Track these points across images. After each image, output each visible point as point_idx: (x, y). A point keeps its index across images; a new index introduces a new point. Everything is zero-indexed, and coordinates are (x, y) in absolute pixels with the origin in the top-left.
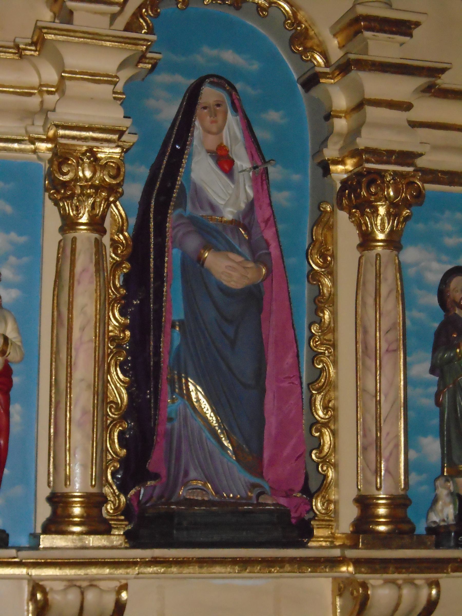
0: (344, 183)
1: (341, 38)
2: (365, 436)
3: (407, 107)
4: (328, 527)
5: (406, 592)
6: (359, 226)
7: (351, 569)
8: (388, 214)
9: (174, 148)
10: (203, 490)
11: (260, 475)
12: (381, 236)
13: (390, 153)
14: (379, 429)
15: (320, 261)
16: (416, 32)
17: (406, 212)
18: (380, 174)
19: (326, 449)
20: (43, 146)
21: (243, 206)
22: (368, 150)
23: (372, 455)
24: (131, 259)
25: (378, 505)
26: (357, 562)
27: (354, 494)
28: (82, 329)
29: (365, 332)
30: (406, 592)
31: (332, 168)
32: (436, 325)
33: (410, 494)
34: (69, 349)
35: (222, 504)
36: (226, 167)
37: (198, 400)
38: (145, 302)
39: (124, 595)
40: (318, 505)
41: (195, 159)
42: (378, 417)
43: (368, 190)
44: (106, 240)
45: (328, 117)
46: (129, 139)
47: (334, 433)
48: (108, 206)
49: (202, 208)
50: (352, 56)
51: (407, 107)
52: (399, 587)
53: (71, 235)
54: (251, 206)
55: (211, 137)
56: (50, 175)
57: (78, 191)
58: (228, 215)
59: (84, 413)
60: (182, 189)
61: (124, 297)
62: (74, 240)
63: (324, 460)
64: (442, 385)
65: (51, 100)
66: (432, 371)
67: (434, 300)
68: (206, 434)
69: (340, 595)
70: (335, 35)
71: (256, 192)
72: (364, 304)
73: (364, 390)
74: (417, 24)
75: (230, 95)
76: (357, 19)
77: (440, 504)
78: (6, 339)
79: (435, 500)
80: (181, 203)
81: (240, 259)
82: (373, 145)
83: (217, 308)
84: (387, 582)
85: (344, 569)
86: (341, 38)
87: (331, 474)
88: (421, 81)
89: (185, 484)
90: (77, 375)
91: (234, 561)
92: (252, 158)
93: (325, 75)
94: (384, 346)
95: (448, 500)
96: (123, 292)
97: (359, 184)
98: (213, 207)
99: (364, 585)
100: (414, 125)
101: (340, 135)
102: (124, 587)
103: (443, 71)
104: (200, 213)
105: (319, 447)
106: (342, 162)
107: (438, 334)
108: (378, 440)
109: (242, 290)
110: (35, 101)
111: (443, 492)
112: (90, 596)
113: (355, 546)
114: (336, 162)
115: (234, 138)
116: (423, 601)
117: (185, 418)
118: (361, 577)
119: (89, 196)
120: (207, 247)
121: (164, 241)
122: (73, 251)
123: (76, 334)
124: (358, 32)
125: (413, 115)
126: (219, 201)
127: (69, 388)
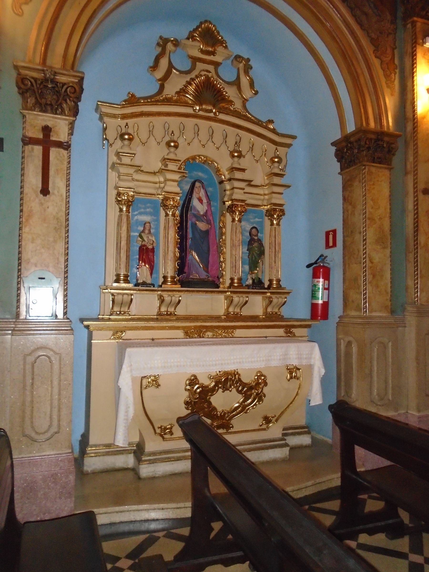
0: (229, 207)
1: (229, 172)
2: (232, 264)
3: (244, 189)
4: (223, 285)
5: (241, 299)
6: (232, 217)
7: (229, 293)
8: (239, 214)
9: (189, 197)
10: (196, 276)
11: (208, 273)
12: (237, 219)
13: (239, 200)
14: (236, 263)
15: (222, 224)
16: (285, 177)
17: (243, 214)
18: (238, 205)
19: (223, 268)
20: (160, 196)
21: (205, 211)
22: (234, 199)
23: (234, 269)
24: (180, 223)
25: (235, 280)
26: (231, 292)
27: (268, 279)
28: (171, 239)
29: (233, 241)
30: (241, 299)
31: (226, 203)
32: (249, 240)
33: (242, 278)
34: (168, 243)
35: (200, 279)
36: (201, 202)
37: (195, 256)
38: (183, 233)
39: (132, 297)
40: (221, 280)
41: (194, 199)
42: (236, 260)
43: (235, 209)
44: (130, 214)
45: (225, 191)
46: (181, 195)
47: (225, 264)
48: (176, 211)
49: (196, 211)
50: (232, 177)
51: (244, 189)
52: (240, 298)
53: (168, 217)
54: (207, 211)
55: (197, 194)
56: (162, 203)
57: (170, 207)
58: (202, 213)
59: (171, 258)
60: (191, 207)
61: (178, 232)
62: (169, 218)
63: (223, 270)
64: (249, 254)
65: (162, 185)
66: (247, 250)
67: (248, 234)
68: (197, 264)
69: (226, 300)
70: (227, 171)
71: (208, 207)
72: (233, 235)
73: (233, 254)
74: (246, 169)
75: (202, 185)
76: (233, 168)
77: (248, 280)
78: (153, 241)
79: (248, 279)
80: (191, 210)
81: (205, 224)
82: (236, 198)
83: (199, 235)
84: (237, 296)
85: (228, 293)
86: (229, 172)
87: (224, 273)
88: (247, 183)
89: (192, 275)
90: (170, 249)
91: (204, 291)
92: (207, 200)
93: (225, 181)
94: (237, 244)
95: (251, 279)
96: (178, 231)
97: (232, 207)
98: (198, 211)
99: (232, 297)
100: (245, 193)
101: (227, 195)
102: (181, 296)
103: (252, 181)
104: (195, 213)
105: (222, 267)
106: (228, 202)
107: (249, 242)
108: (236, 265)
109: (205, 231)
110: (157, 185)
111: (249, 277)
112: (173, 298)
113: (231, 288)
114: (227, 201)
115: (202, 195)
116: (245, 301)
117: (192, 260)
118: (232, 295)
119: (172, 208)
120: (198, 221)
121: (187, 219)
122: (169, 221)
123: (169, 240)
124: (233, 171)
125: (245, 191)
126: (200, 210)
127: (168, 253)
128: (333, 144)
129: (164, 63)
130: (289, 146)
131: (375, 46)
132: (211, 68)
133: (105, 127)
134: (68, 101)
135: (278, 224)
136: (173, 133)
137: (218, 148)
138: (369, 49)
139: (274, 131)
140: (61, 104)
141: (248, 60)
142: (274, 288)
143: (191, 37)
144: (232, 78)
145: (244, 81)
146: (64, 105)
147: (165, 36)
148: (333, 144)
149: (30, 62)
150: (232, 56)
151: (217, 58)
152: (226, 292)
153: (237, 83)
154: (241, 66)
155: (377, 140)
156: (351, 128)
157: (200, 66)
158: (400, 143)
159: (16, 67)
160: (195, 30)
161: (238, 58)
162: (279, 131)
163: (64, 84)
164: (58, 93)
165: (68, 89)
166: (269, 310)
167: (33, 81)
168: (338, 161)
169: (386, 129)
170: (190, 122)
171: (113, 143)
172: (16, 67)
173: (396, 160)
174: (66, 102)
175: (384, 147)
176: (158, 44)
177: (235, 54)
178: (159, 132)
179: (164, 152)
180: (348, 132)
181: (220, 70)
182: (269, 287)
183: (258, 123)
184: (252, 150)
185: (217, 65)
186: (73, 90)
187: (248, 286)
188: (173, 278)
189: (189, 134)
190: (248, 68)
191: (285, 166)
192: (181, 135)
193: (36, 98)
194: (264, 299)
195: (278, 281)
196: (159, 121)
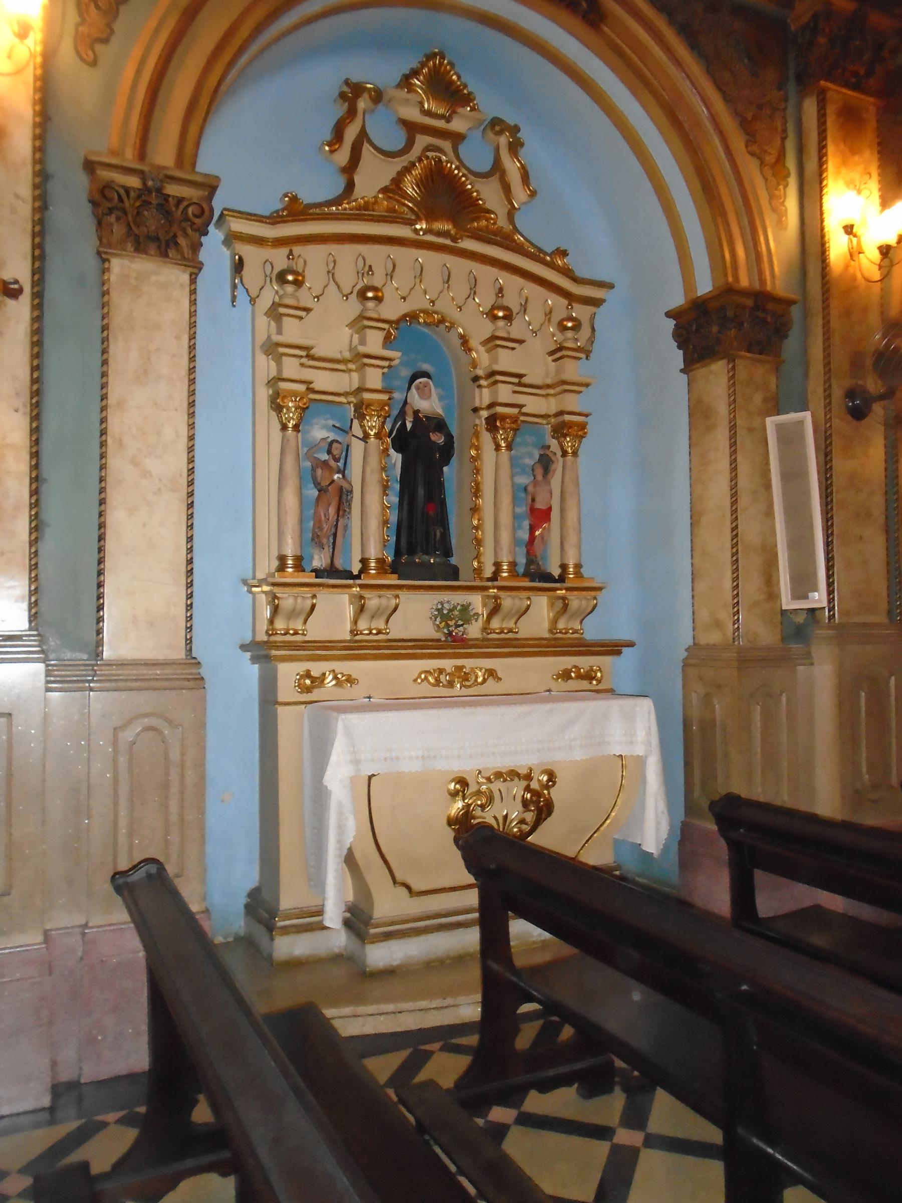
103: (525, 375)
128: (668, 314)
129: (351, 133)
130: (596, 303)
131: (748, 134)
132: (446, 145)
133: (237, 261)
134: (189, 231)
135: (575, 454)
136: (372, 271)
137: (460, 308)
138: (738, 142)
139: (567, 273)
140: (175, 236)
141: (515, 130)
142: (504, 579)
143: (406, 82)
144: (485, 165)
145: (512, 167)
146: (182, 241)
147: (355, 78)
148: (668, 314)
149: (113, 153)
150: (485, 120)
151: (457, 125)
152: (486, 588)
153: (497, 169)
154: (503, 140)
155: (756, 307)
156: (704, 286)
157: (422, 141)
158: (795, 312)
159: (90, 166)
160: (415, 73)
161: (497, 125)
162: (580, 273)
163: (180, 200)
164: (167, 214)
165: (190, 210)
166: (561, 625)
167: (122, 192)
168: (679, 347)
169: (769, 287)
170: (405, 256)
171: (258, 297)
172: (90, 166)
173: (791, 344)
174: (186, 235)
175: (767, 322)
176: (342, 96)
177: (491, 117)
178: (348, 278)
179: (354, 307)
180: (699, 294)
181: (462, 149)
182: (495, 577)
183: (537, 256)
184: (525, 310)
185: (457, 138)
186: (198, 212)
187: (318, 573)
188: (381, 562)
189: (402, 281)
190: (515, 147)
191: (591, 340)
192: (389, 282)
193: (129, 225)
194: (552, 605)
195: (578, 566)
196: (347, 253)
